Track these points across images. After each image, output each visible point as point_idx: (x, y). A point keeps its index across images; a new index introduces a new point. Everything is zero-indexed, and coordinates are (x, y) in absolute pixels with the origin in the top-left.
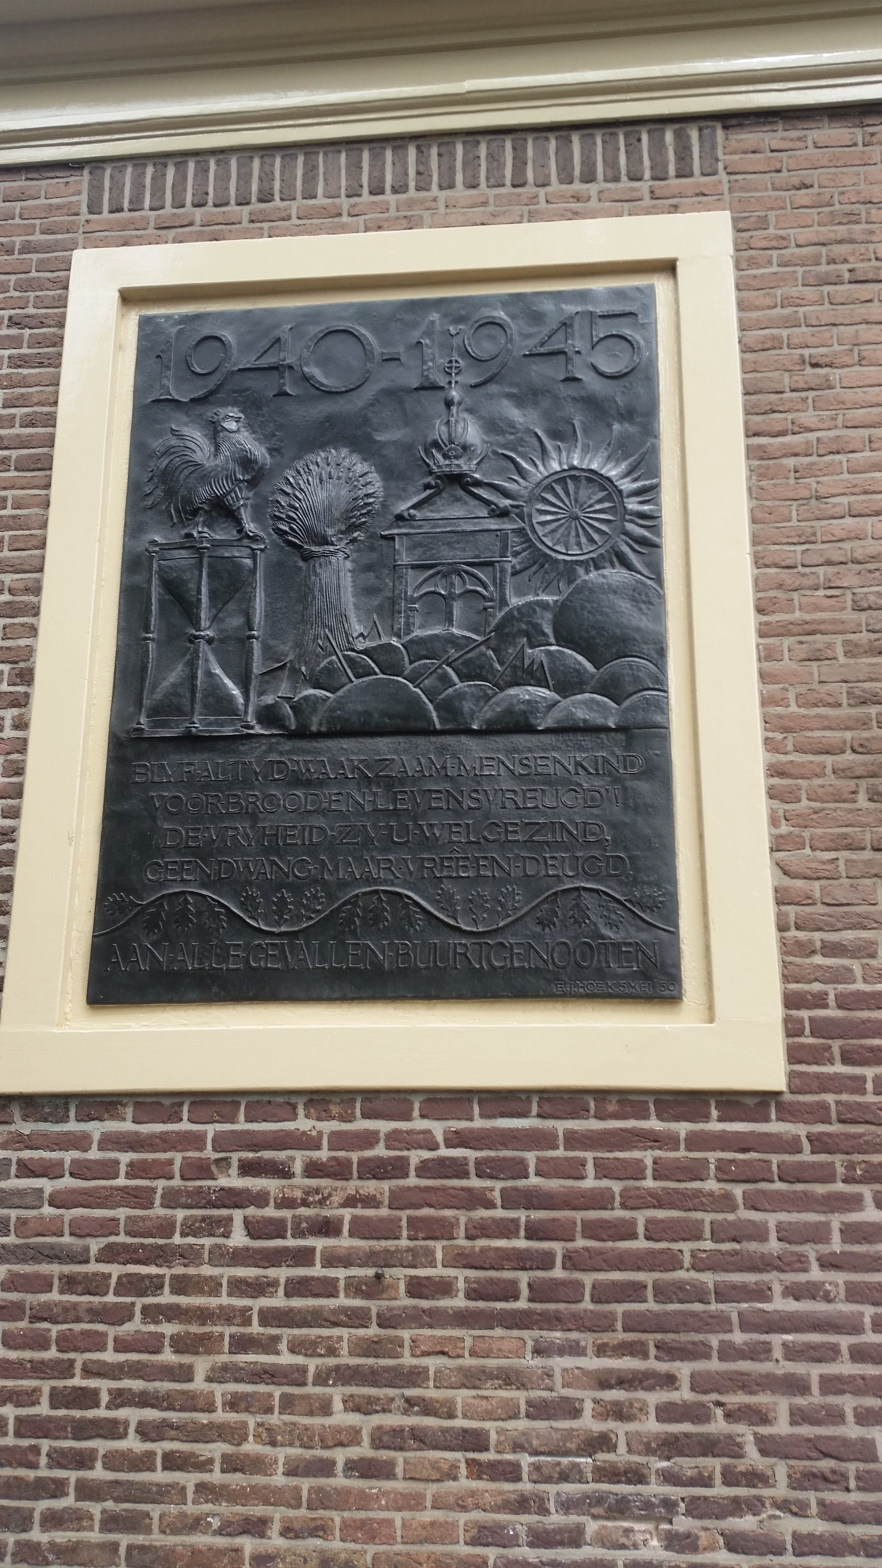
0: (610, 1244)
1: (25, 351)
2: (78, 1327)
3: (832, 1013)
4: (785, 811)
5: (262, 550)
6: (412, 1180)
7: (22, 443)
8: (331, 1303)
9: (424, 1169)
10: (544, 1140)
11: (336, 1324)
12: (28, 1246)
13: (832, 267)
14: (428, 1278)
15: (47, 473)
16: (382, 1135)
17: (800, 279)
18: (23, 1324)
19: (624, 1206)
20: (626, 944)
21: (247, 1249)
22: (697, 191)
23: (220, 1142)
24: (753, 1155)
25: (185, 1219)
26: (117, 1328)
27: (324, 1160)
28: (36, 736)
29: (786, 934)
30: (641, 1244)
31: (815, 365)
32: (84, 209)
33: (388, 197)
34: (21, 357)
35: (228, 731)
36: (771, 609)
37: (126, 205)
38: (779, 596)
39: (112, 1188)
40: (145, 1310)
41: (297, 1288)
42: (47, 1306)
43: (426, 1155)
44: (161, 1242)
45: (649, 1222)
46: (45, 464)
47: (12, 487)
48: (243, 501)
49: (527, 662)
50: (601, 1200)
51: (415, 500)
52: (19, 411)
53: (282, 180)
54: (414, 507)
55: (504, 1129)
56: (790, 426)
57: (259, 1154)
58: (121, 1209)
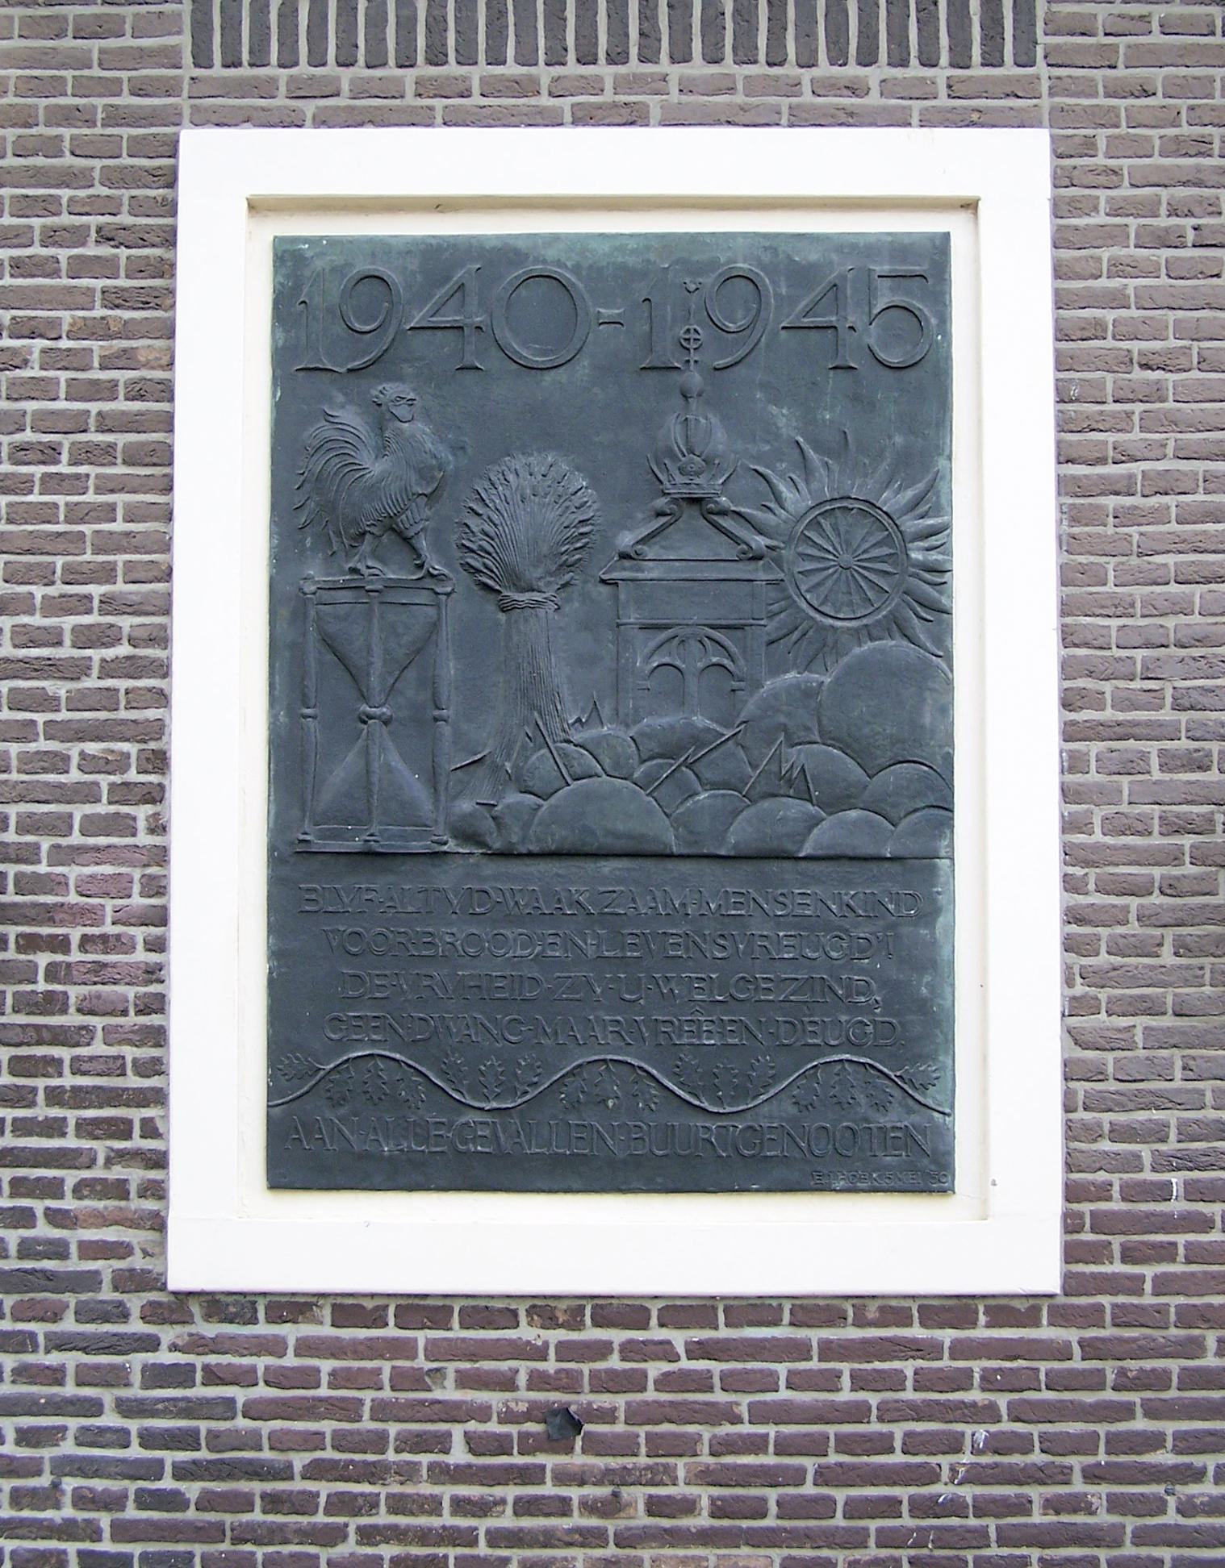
0: (865, 1459)
1: (123, 282)
2: (287, 1549)
3: (1116, 1205)
4: (1082, 967)
5: (448, 594)
6: (651, 1395)
7: (131, 424)
8: (565, 1523)
9: (665, 1382)
10: (800, 1350)
11: (570, 1544)
12: (222, 1461)
13: (1174, 221)
14: (669, 1497)
15: (166, 470)
16: (616, 1346)
17: (1132, 236)
18: (226, 1546)
19: (881, 1419)
20: (895, 1128)
21: (469, 1466)
22: (1008, 90)
23: (435, 1351)
24: (1021, 1363)
25: (398, 1434)
26: (330, 1550)
27: (552, 1372)
28: (179, 842)
29: (1072, 1116)
30: (898, 1458)
31: (1145, 366)
32: (187, 59)
33: (603, 70)
34: (119, 291)
35: (416, 846)
36: (1079, 704)
37: (245, 57)
38: (1089, 686)
39: (314, 1399)
40: (360, 1530)
41: (525, 1507)
42: (251, 1527)
43: (666, 1367)
44: (371, 1457)
45: (908, 1435)
46: (164, 456)
47: (121, 490)
48: (420, 519)
49: (785, 767)
50: (858, 1413)
51: (645, 531)
52: (122, 376)
53: (457, 32)
54: (643, 541)
55: (752, 1339)
56: (1111, 453)
57: (477, 1365)
58: (326, 1422)
